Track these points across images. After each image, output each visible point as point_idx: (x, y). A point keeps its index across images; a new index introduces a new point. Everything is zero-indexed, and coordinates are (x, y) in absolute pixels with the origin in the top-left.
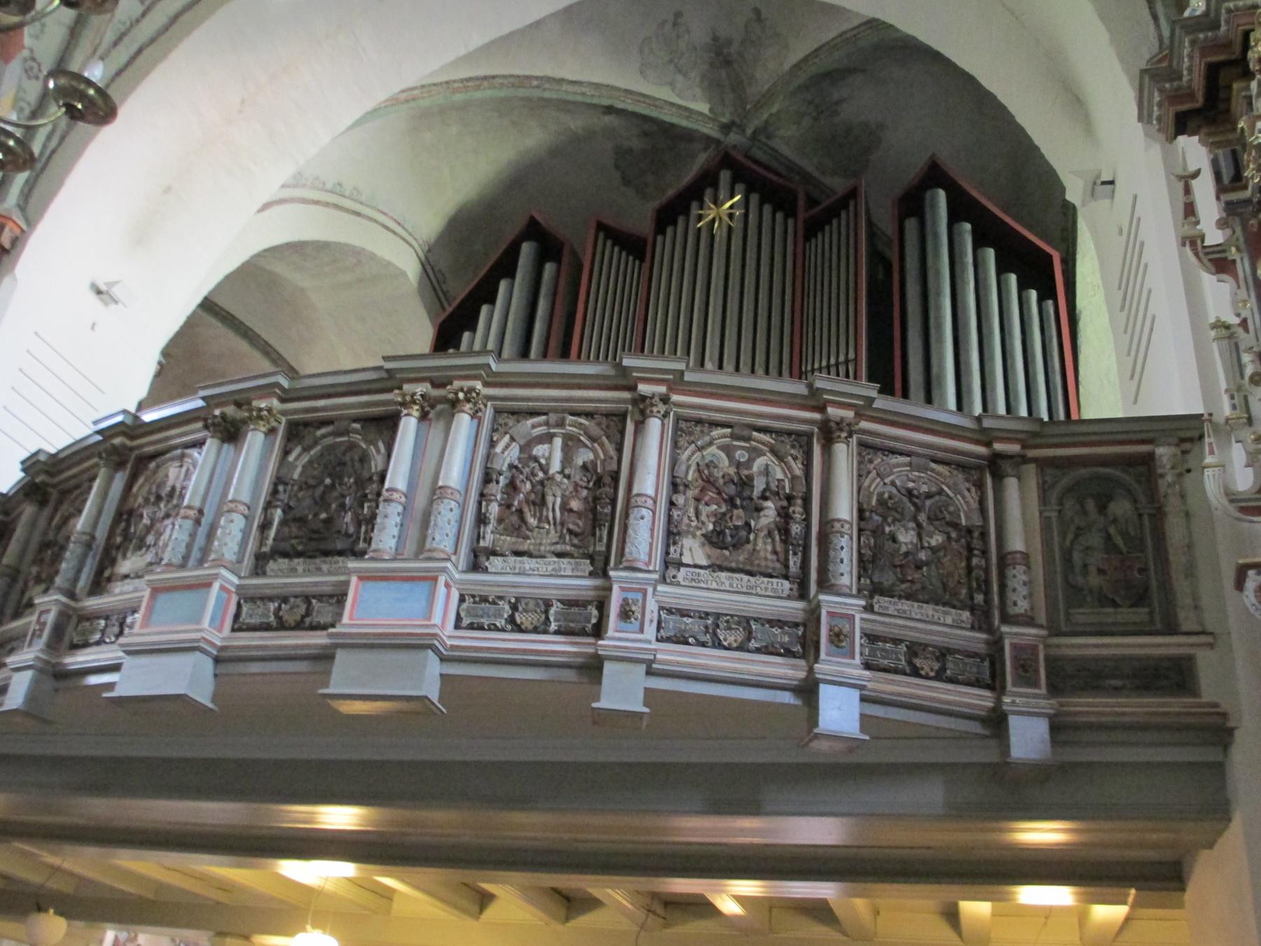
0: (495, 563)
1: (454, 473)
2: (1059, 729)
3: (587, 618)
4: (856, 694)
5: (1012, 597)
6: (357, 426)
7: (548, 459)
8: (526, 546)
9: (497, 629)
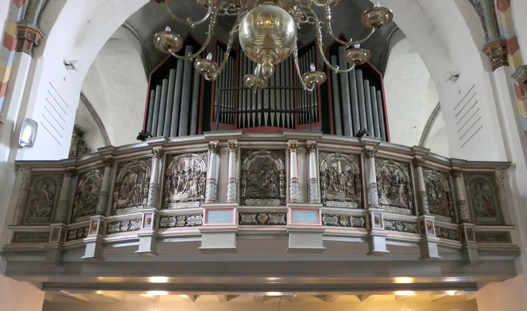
0: (328, 203)
1: (313, 173)
2: (480, 252)
3: (365, 223)
4: (436, 244)
5: (463, 214)
6: (269, 152)
7: (337, 168)
8: (336, 198)
9: (335, 225)
